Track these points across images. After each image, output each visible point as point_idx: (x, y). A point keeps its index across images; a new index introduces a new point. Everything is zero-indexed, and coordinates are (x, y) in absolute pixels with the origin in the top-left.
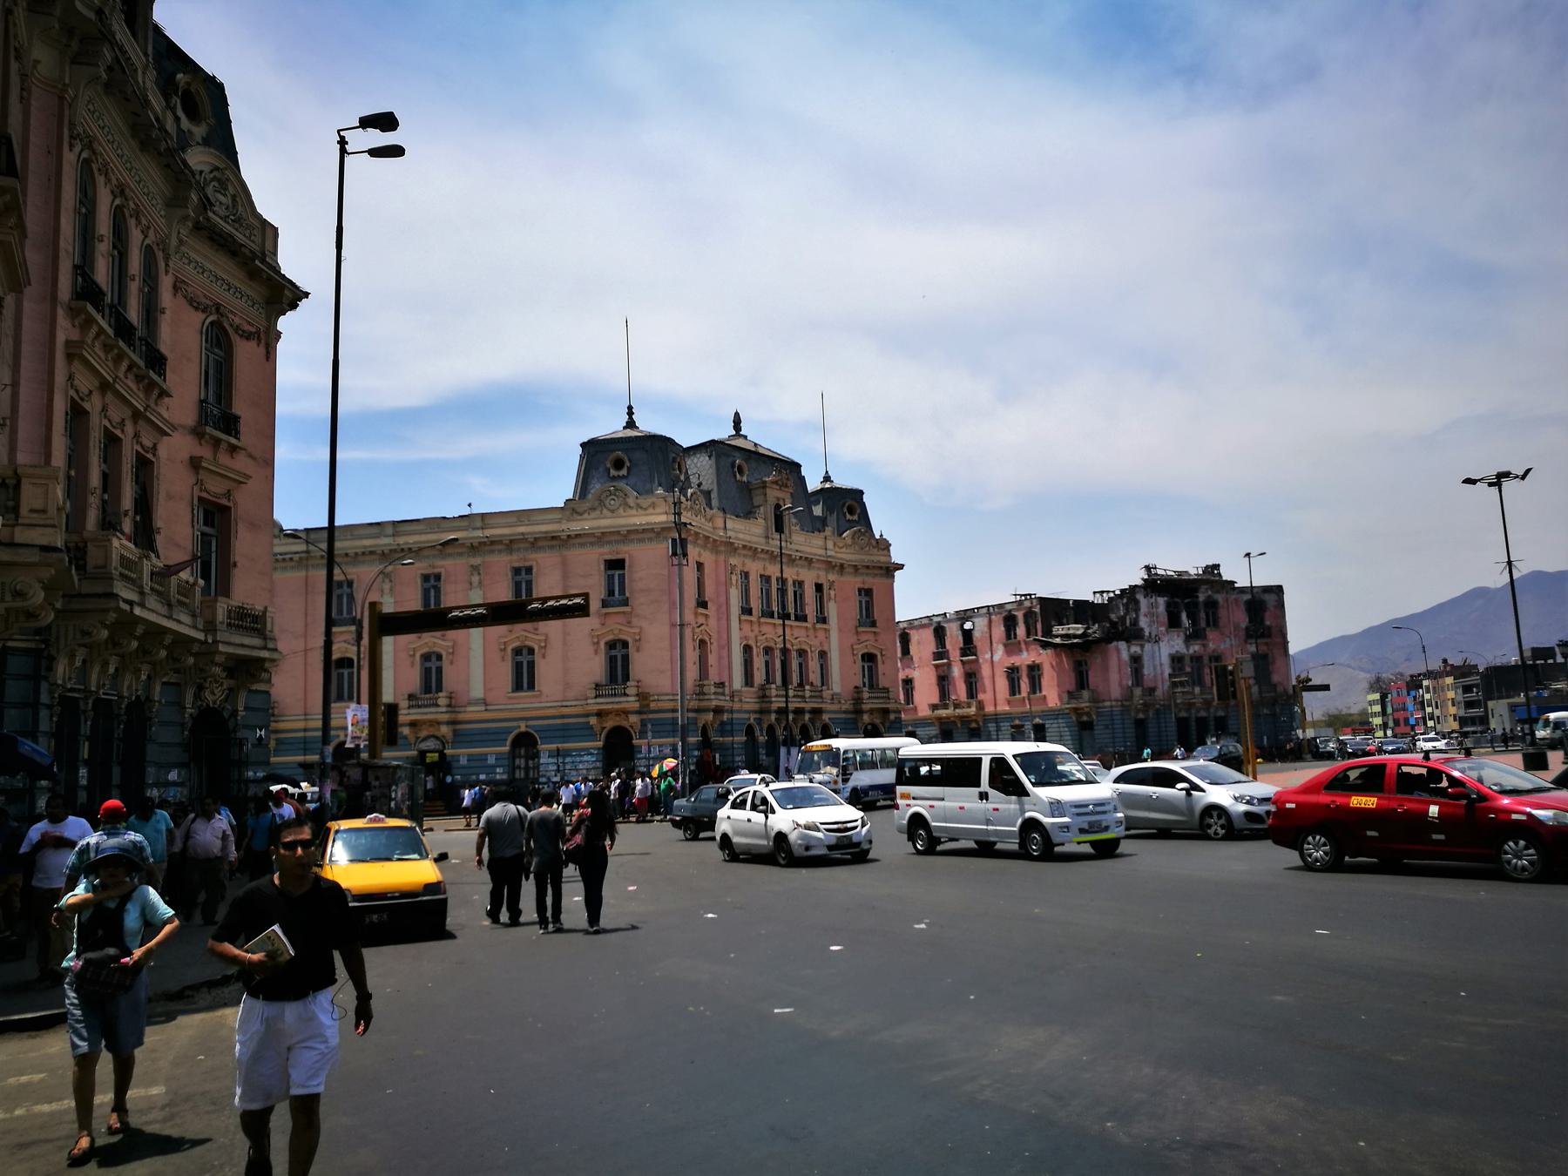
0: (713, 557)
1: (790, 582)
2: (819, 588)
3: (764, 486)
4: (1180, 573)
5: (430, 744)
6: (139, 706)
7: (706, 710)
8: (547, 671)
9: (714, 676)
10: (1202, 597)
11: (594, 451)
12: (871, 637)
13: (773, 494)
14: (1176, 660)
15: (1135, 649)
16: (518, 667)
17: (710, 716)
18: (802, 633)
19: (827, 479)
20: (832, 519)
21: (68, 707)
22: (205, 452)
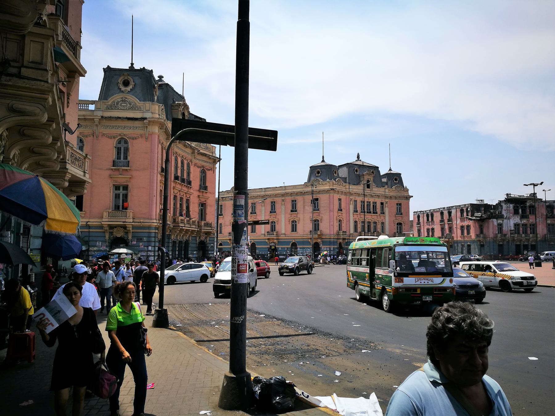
0: (345, 197)
1: (372, 202)
2: (382, 204)
3: (363, 175)
4: (520, 196)
5: (272, 244)
6: (187, 242)
7: (340, 239)
8: (299, 227)
9: (344, 229)
10: (528, 204)
11: (313, 168)
12: (401, 218)
13: (366, 178)
14: (516, 225)
15: (500, 221)
16: (293, 225)
17: (341, 241)
18: (376, 217)
19: (390, 170)
20: (389, 183)
21: (174, 242)
22: (201, 194)
